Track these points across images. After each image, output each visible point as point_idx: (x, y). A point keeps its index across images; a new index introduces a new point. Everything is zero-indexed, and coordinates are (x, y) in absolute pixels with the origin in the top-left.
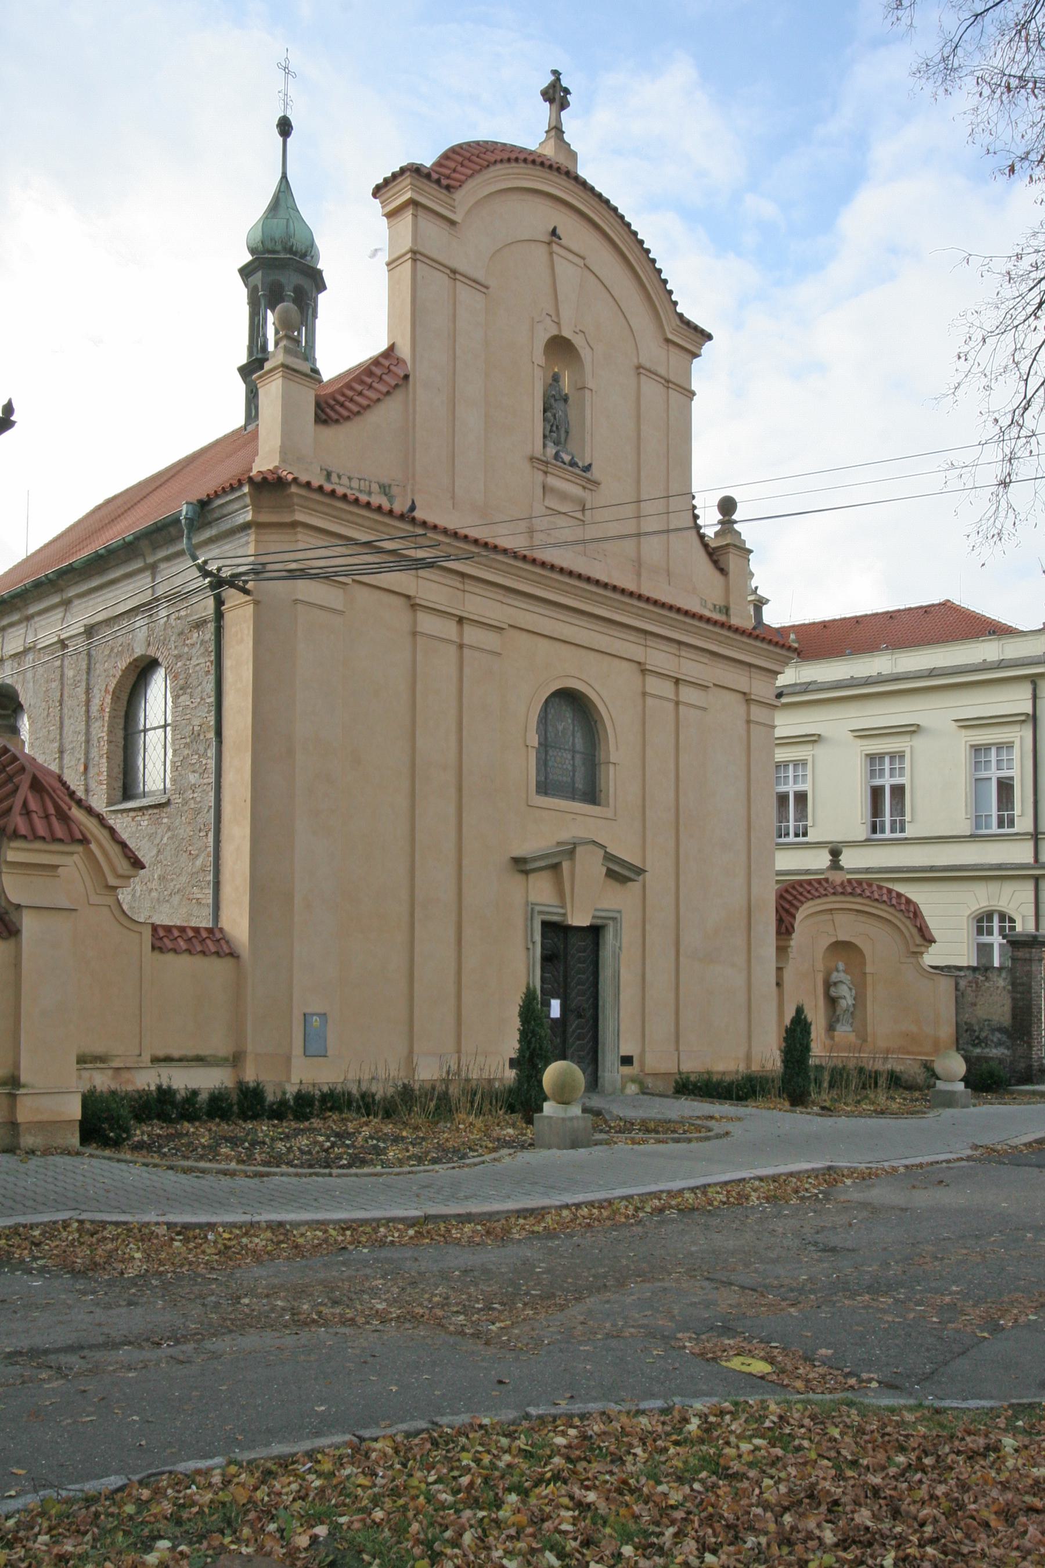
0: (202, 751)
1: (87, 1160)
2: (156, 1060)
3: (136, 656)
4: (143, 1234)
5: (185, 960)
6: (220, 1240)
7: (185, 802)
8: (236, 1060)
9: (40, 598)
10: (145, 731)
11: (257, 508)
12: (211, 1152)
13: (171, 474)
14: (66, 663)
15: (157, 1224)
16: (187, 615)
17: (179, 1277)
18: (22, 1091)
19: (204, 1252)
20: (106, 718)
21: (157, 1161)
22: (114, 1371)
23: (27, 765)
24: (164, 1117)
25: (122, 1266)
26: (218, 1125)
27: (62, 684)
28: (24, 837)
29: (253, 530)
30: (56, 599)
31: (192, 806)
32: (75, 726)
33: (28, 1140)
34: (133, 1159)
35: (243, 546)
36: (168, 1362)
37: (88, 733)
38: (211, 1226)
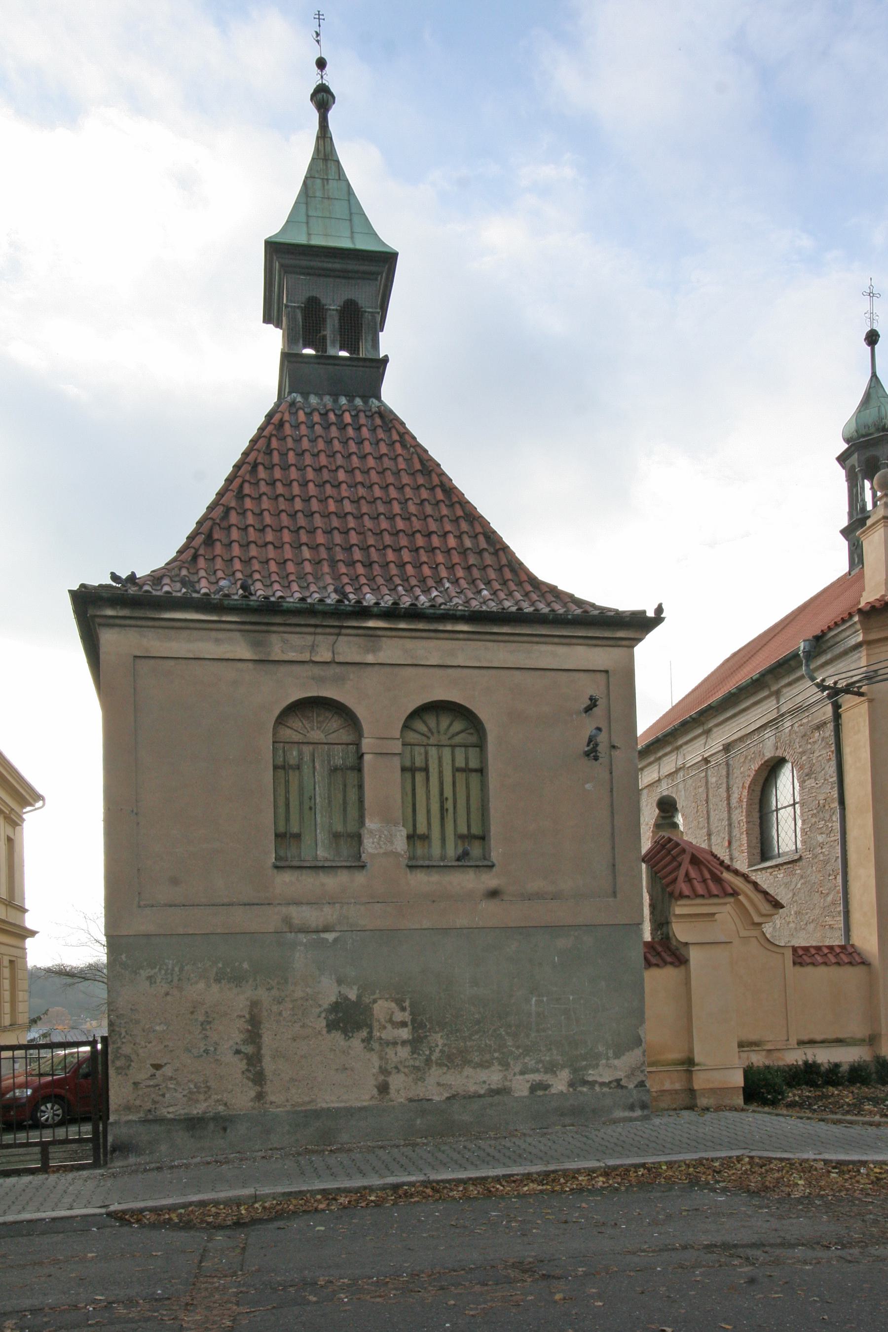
0: (827, 816)
1: (751, 1115)
2: (801, 1043)
3: (766, 758)
4: (805, 1167)
5: (822, 969)
6: (871, 1174)
7: (815, 856)
8: (872, 1040)
9: (686, 733)
10: (777, 810)
11: (866, 630)
12: (857, 1108)
13: (786, 622)
14: (709, 773)
15: (815, 1160)
16: (808, 722)
17: (840, 1200)
18: (696, 1068)
19: (858, 1182)
20: (744, 806)
21: (810, 1115)
22: (793, 1263)
23: (687, 847)
24: (812, 1084)
25: (788, 1189)
26: (860, 1088)
27: (707, 788)
28: (688, 897)
29: (864, 647)
30: (699, 731)
31: (822, 858)
32: (719, 816)
33: (703, 1102)
34: (790, 1113)
35: (856, 661)
36: (838, 1261)
37: (730, 819)
38: (864, 1163)
